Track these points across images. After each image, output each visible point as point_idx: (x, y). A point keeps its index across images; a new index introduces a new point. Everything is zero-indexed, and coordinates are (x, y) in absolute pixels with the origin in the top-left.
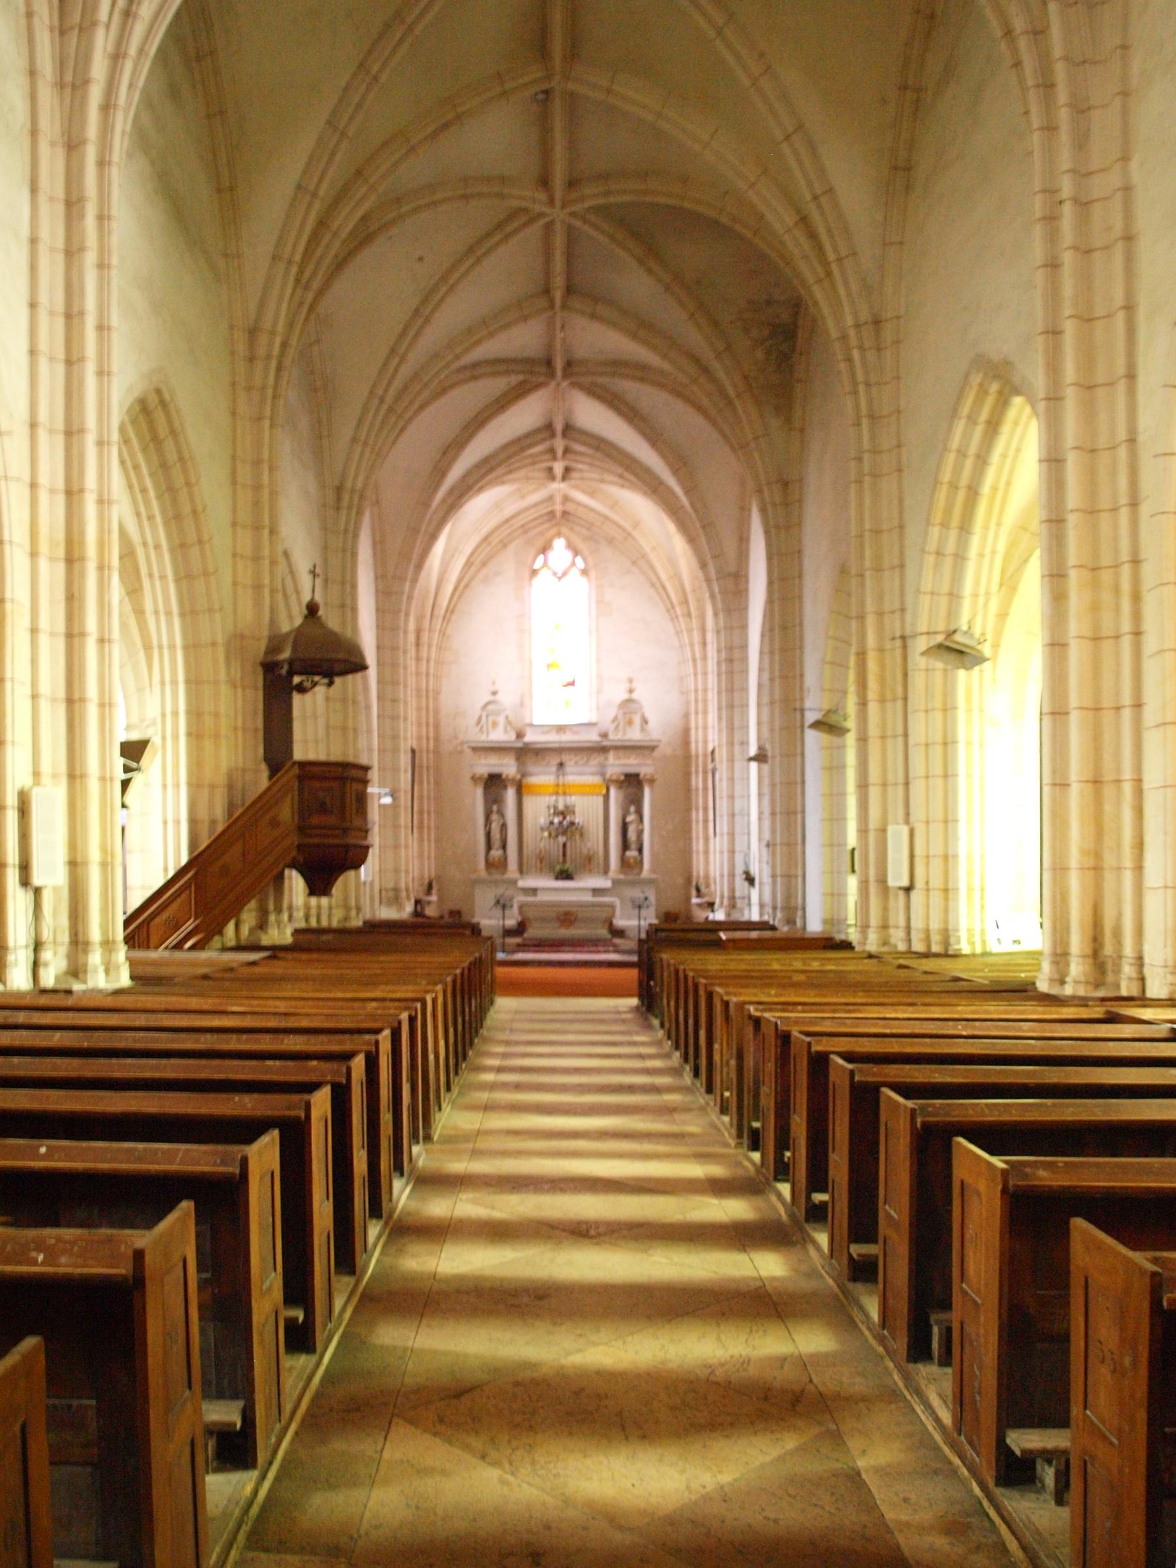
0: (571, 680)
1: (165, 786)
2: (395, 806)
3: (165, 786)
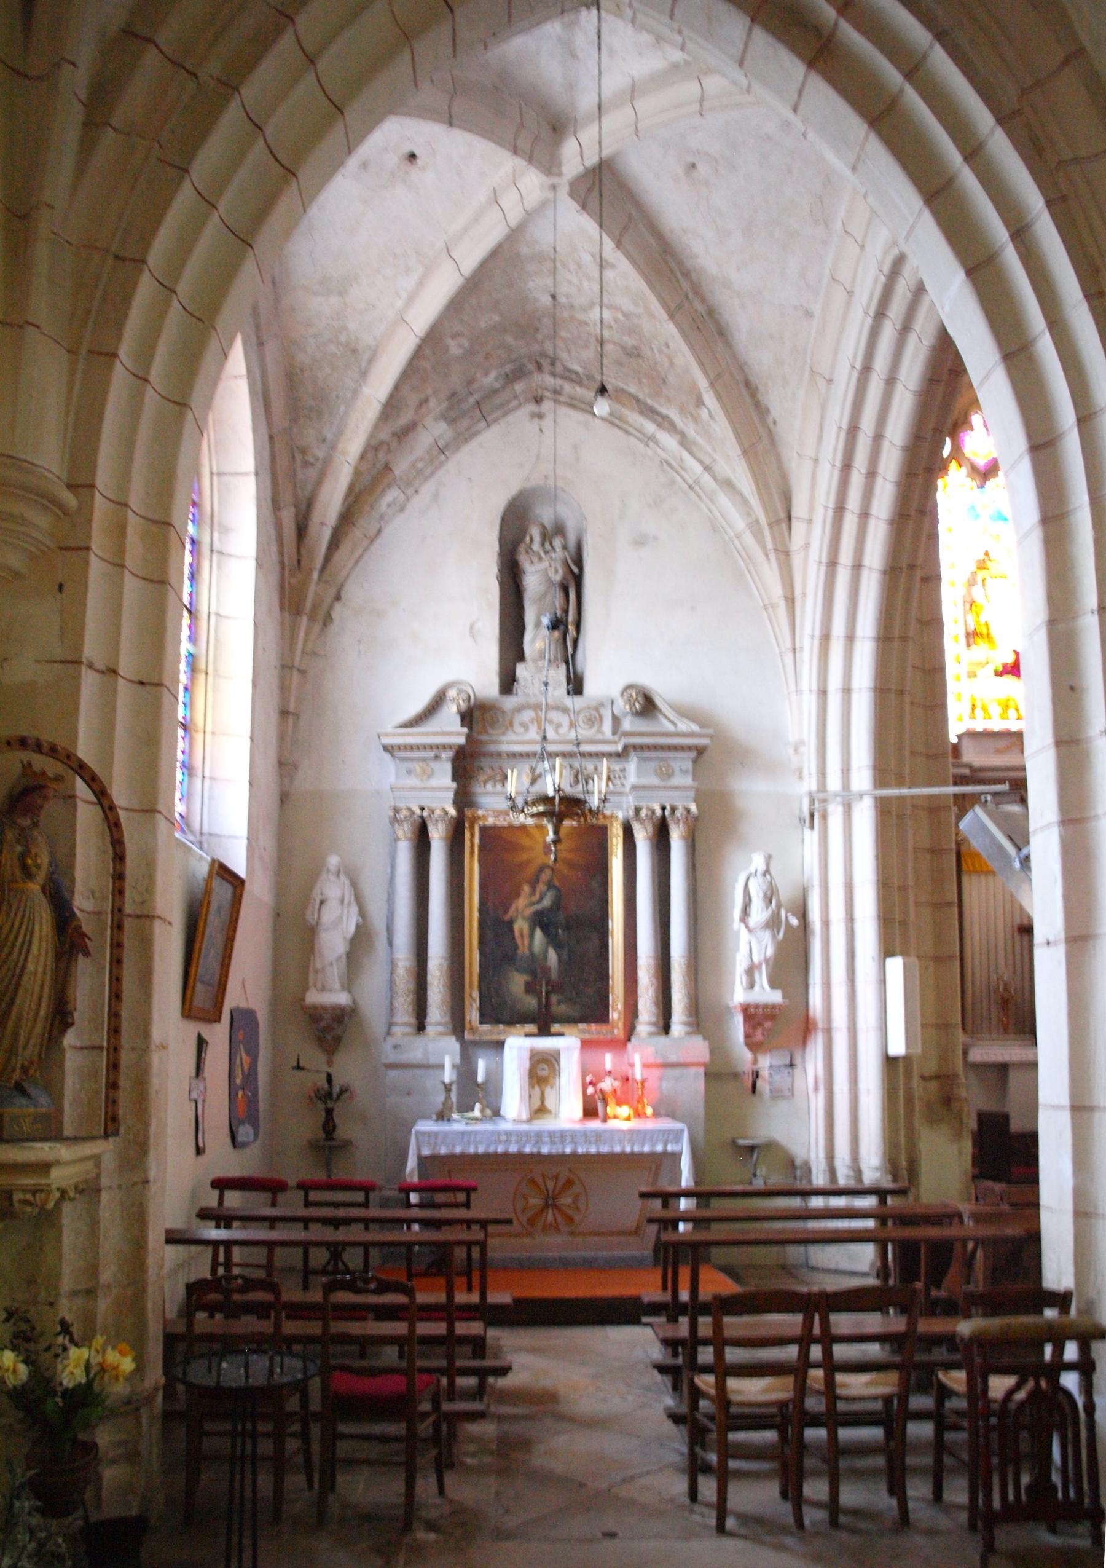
0: (1010, 659)
1: (826, 638)
2: (408, 1205)
3: (823, 693)
